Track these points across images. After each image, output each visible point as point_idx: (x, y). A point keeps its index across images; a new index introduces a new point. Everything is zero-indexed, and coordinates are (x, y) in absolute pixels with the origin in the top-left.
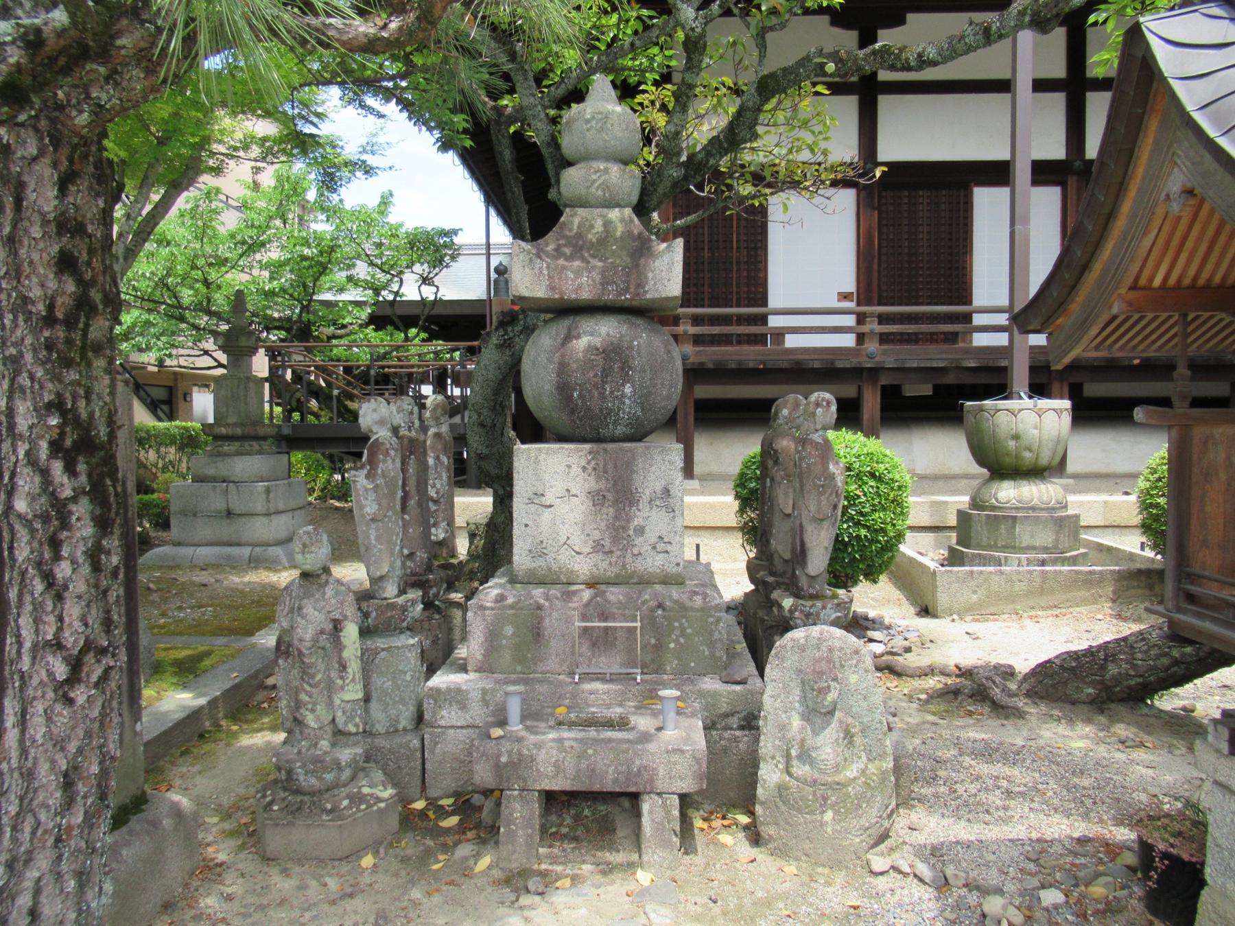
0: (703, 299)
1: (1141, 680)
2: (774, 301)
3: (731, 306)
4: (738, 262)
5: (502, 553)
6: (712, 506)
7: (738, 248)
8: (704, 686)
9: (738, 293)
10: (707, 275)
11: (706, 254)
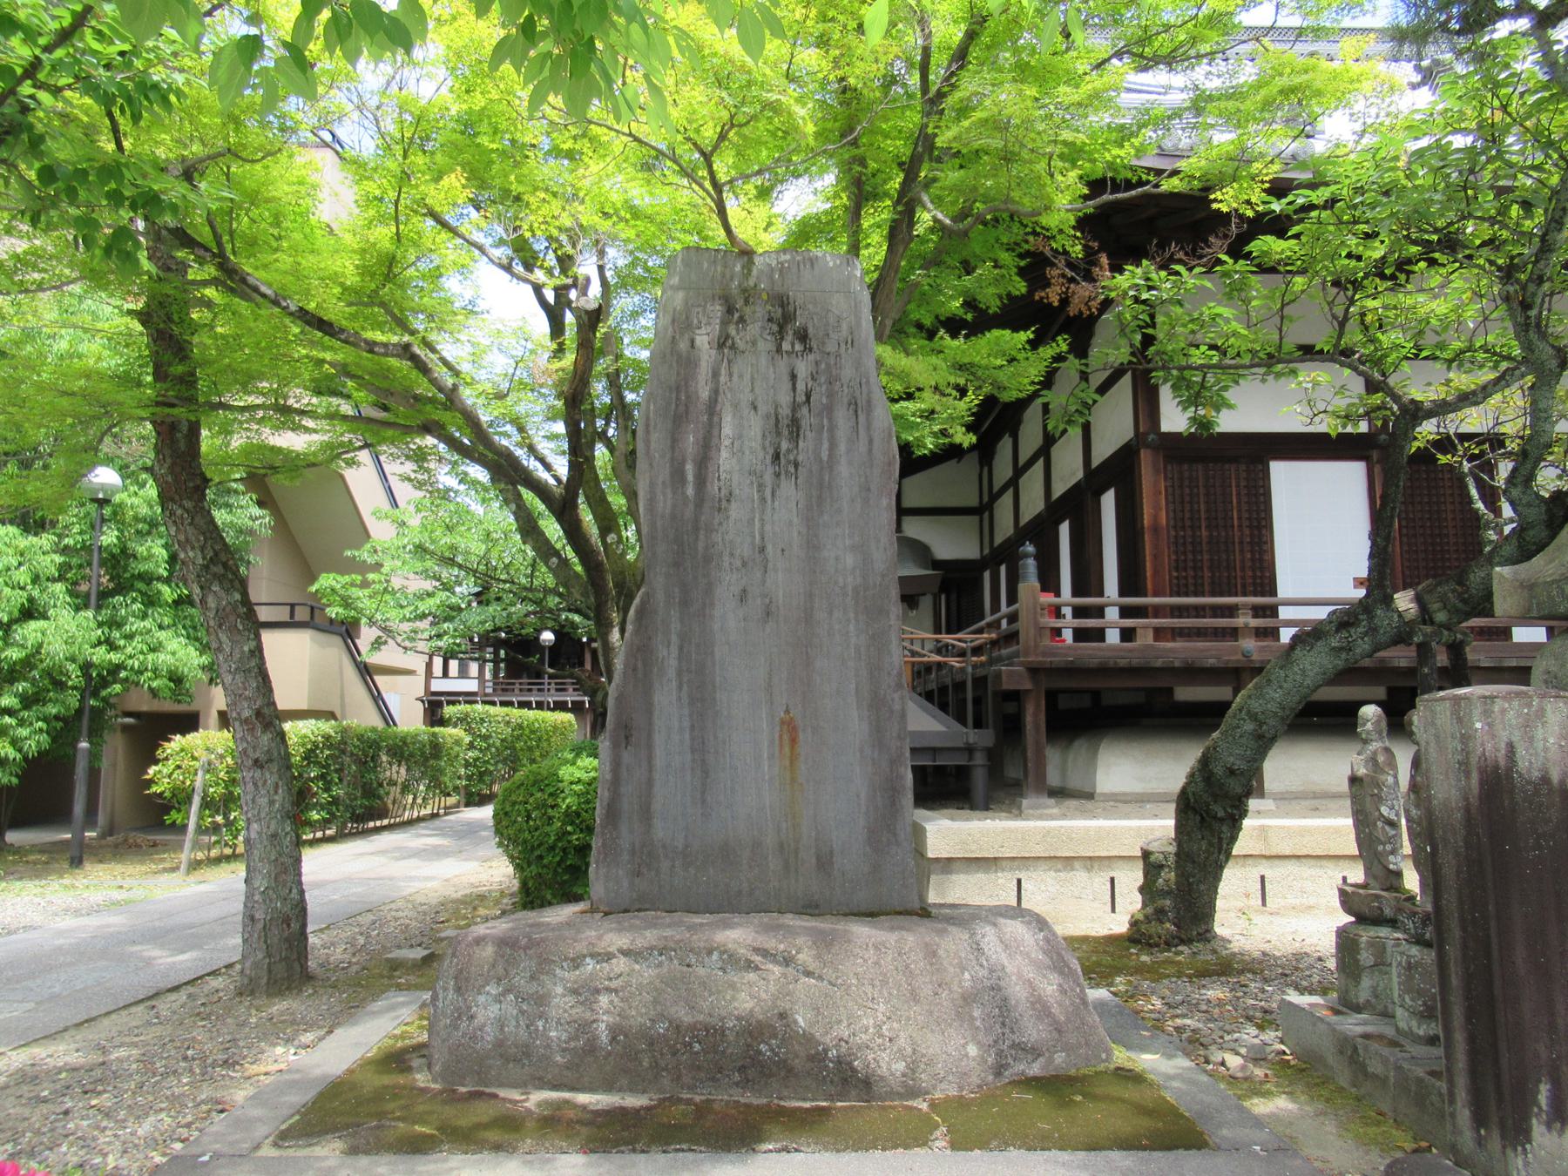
0: (1186, 585)
1: (326, 727)
2: (1285, 589)
3: (1164, 595)
4: (1241, 543)
5: (1202, 887)
6: (1302, 832)
7: (1240, 526)
8: (1287, 998)
9: (1243, 578)
10: (1206, 557)
11: (1204, 533)
